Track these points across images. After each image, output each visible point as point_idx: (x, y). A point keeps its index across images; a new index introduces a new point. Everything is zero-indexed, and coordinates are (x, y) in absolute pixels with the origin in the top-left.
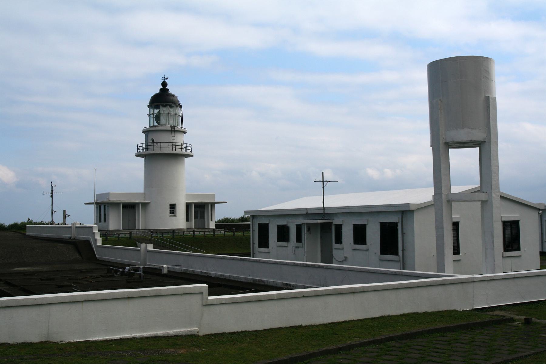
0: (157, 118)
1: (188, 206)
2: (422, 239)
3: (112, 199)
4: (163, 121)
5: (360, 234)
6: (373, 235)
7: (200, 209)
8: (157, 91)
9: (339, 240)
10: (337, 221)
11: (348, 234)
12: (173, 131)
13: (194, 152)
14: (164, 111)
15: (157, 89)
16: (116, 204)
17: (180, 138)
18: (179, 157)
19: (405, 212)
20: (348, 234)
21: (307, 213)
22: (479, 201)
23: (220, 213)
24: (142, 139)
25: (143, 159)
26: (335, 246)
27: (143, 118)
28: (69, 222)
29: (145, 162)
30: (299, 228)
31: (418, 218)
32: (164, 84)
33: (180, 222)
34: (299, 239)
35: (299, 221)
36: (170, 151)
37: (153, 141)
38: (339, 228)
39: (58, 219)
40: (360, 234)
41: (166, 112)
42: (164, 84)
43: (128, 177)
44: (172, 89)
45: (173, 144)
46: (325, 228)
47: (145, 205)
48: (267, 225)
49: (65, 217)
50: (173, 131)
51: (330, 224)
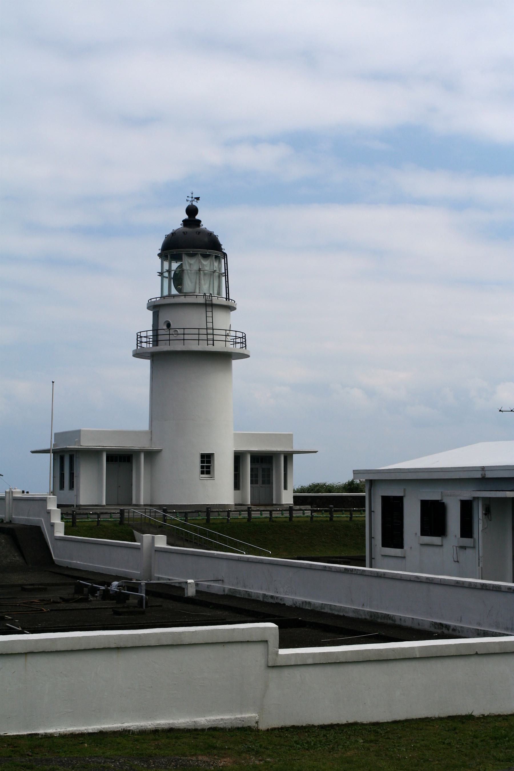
1: (238, 457)
3: (86, 443)
4: (188, 285)
7: (262, 466)
14: (191, 264)
15: (176, 220)
16: (93, 453)
23: (303, 475)
24: (146, 322)
27: (146, 278)
30: (467, 507)
32: (192, 211)
33: (221, 491)
34: (467, 530)
35: (467, 494)
36: (203, 347)
37: (169, 325)
38: (393, 508)
41: (196, 268)
42: (192, 211)
43: (117, 400)
44: (208, 220)
45: (209, 332)
47: (151, 455)
48: (400, 500)
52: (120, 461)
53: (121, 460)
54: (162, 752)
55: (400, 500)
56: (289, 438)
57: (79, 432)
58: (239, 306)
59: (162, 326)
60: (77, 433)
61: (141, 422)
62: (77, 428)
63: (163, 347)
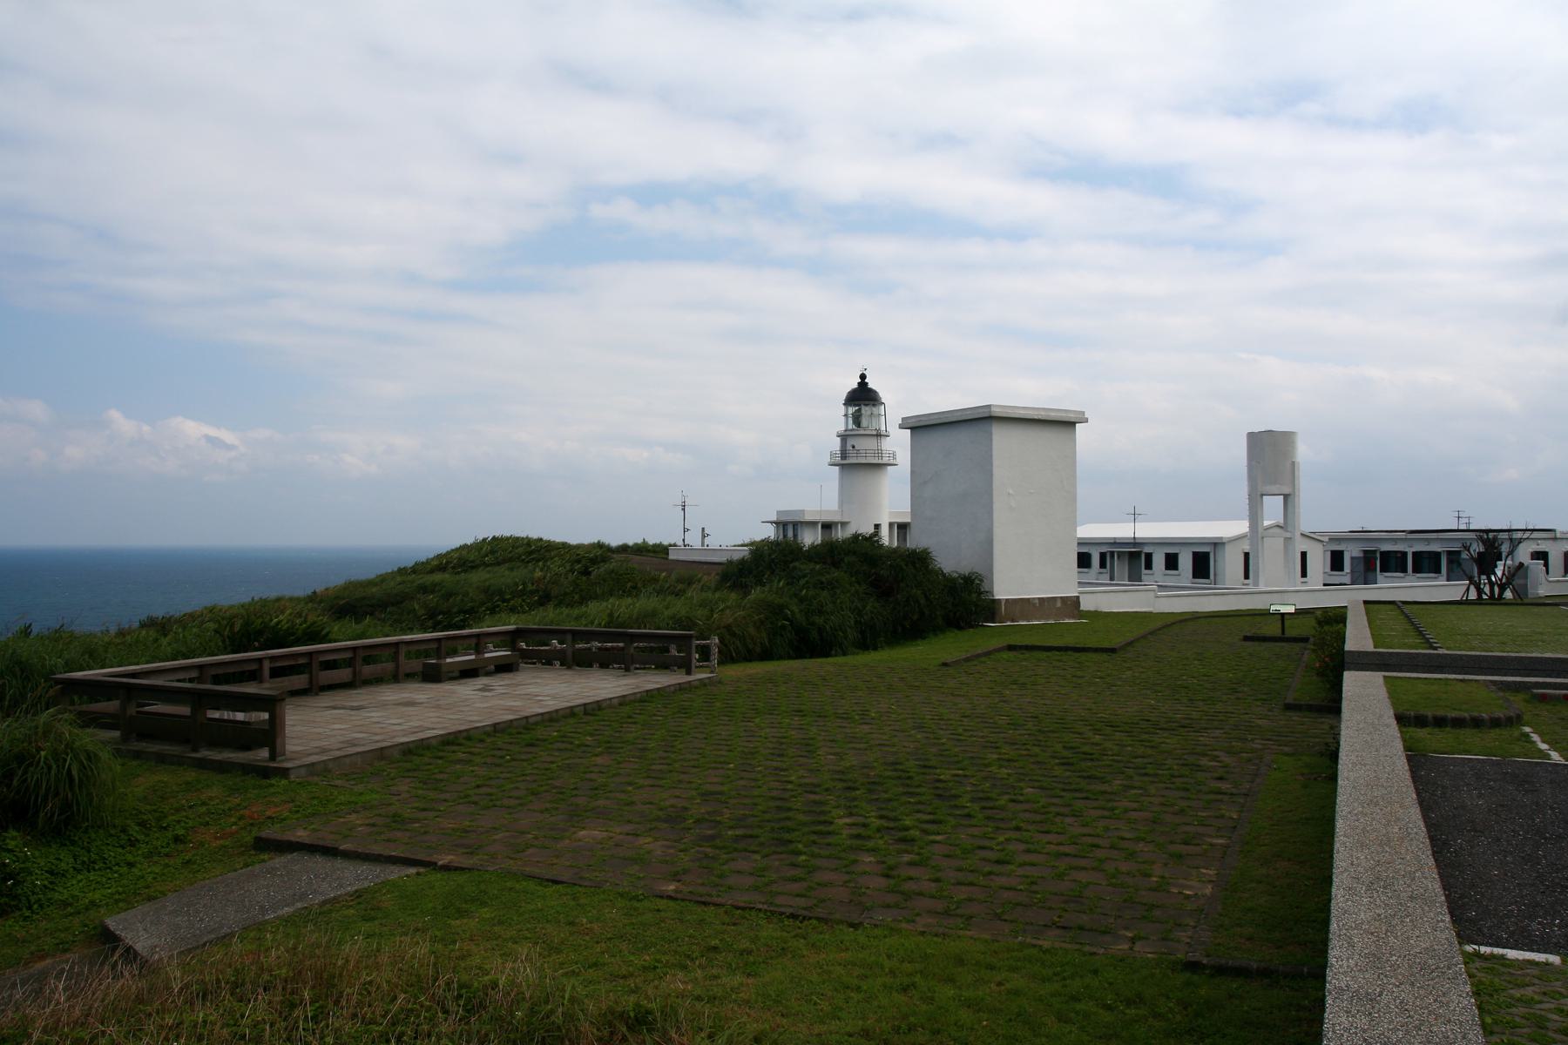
0: (857, 419)
1: (891, 525)
2: (1229, 566)
3: (808, 518)
4: (864, 423)
5: (1172, 562)
6: (1186, 562)
9: (1149, 566)
10: (1147, 550)
11: (1159, 561)
12: (879, 435)
14: (866, 410)
15: (854, 383)
16: (813, 524)
19: (1217, 544)
20: (1159, 561)
21: (1115, 543)
22: (1541, 603)
24: (836, 444)
25: (872, 530)
26: (1144, 571)
27: (837, 418)
28: (713, 543)
30: (1103, 556)
31: (1228, 548)
32: (863, 377)
34: (1103, 565)
35: (1104, 549)
36: (876, 461)
38: (1149, 557)
39: (694, 540)
40: (1172, 562)
42: (863, 377)
44: (872, 383)
45: (879, 453)
46: (1133, 556)
48: (1341, 553)
49: (704, 536)
50: (879, 435)
51: (1139, 553)
52: (1416, 570)
53: (827, 526)
55: (1341, 553)
59: (849, 447)
60: (803, 512)
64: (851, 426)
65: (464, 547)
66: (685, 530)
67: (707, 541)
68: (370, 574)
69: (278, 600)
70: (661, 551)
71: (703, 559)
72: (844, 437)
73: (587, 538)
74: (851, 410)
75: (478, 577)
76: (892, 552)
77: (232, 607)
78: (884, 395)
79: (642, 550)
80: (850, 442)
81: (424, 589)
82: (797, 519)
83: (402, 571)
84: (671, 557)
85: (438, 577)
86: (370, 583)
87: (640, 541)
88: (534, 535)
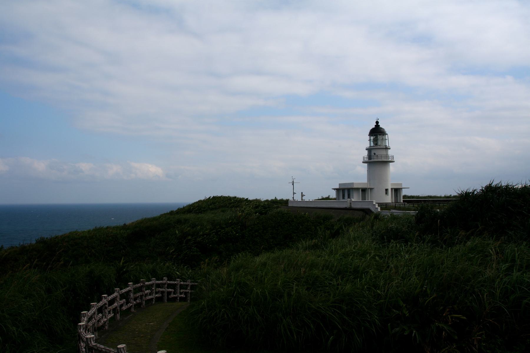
0: (376, 141)
1: (392, 189)
3: (355, 186)
4: (379, 143)
7: (397, 191)
8: (374, 127)
13: (395, 160)
14: (380, 137)
15: (373, 126)
16: (357, 189)
17: (389, 151)
18: (386, 163)
23: (404, 192)
24: (366, 153)
25: (366, 164)
27: (366, 142)
28: (306, 199)
29: (368, 166)
32: (377, 122)
33: (389, 199)
36: (386, 160)
37: (375, 154)
39: (298, 198)
41: (381, 138)
42: (377, 122)
43: (358, 174)
44: (381, 125)
45: (387, 156)
47: (371, 189)
54: (348, 287)
56: (401, 184)
57: (288, 200)
58: (391, 148)
59: (372, 154)
60: (353, 184)
61: (365, 181)
62: (288, 198)
63: (372, 160)
64: (372, 144)
65: (200, 201)
66: (294, 193)
67: (304, 198)
68: (157, 214)
69: (107, 228)
70: (285, 202)
71: (305, 206)
72: (369, 150)
73: (270, 198)
74: (372, 138)
75: (208, 216)
76: (80, 313)
77: (84, 232)
78: (387, 130)
79: (275, 203)
80: (373, 152)
81: (179, 222)
82: (350, 187)
83: (172, 213)
84: (289, 205)
85: (188, 216)
86: (155, 219)
87: (274, 198)
88: (232, 195)
